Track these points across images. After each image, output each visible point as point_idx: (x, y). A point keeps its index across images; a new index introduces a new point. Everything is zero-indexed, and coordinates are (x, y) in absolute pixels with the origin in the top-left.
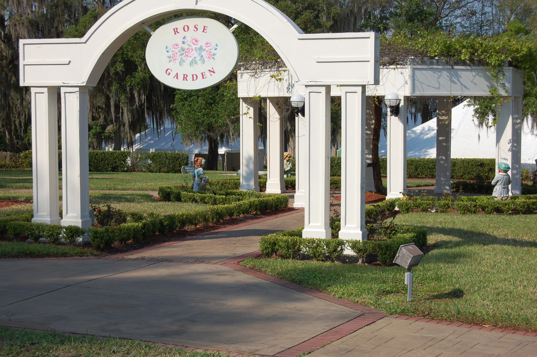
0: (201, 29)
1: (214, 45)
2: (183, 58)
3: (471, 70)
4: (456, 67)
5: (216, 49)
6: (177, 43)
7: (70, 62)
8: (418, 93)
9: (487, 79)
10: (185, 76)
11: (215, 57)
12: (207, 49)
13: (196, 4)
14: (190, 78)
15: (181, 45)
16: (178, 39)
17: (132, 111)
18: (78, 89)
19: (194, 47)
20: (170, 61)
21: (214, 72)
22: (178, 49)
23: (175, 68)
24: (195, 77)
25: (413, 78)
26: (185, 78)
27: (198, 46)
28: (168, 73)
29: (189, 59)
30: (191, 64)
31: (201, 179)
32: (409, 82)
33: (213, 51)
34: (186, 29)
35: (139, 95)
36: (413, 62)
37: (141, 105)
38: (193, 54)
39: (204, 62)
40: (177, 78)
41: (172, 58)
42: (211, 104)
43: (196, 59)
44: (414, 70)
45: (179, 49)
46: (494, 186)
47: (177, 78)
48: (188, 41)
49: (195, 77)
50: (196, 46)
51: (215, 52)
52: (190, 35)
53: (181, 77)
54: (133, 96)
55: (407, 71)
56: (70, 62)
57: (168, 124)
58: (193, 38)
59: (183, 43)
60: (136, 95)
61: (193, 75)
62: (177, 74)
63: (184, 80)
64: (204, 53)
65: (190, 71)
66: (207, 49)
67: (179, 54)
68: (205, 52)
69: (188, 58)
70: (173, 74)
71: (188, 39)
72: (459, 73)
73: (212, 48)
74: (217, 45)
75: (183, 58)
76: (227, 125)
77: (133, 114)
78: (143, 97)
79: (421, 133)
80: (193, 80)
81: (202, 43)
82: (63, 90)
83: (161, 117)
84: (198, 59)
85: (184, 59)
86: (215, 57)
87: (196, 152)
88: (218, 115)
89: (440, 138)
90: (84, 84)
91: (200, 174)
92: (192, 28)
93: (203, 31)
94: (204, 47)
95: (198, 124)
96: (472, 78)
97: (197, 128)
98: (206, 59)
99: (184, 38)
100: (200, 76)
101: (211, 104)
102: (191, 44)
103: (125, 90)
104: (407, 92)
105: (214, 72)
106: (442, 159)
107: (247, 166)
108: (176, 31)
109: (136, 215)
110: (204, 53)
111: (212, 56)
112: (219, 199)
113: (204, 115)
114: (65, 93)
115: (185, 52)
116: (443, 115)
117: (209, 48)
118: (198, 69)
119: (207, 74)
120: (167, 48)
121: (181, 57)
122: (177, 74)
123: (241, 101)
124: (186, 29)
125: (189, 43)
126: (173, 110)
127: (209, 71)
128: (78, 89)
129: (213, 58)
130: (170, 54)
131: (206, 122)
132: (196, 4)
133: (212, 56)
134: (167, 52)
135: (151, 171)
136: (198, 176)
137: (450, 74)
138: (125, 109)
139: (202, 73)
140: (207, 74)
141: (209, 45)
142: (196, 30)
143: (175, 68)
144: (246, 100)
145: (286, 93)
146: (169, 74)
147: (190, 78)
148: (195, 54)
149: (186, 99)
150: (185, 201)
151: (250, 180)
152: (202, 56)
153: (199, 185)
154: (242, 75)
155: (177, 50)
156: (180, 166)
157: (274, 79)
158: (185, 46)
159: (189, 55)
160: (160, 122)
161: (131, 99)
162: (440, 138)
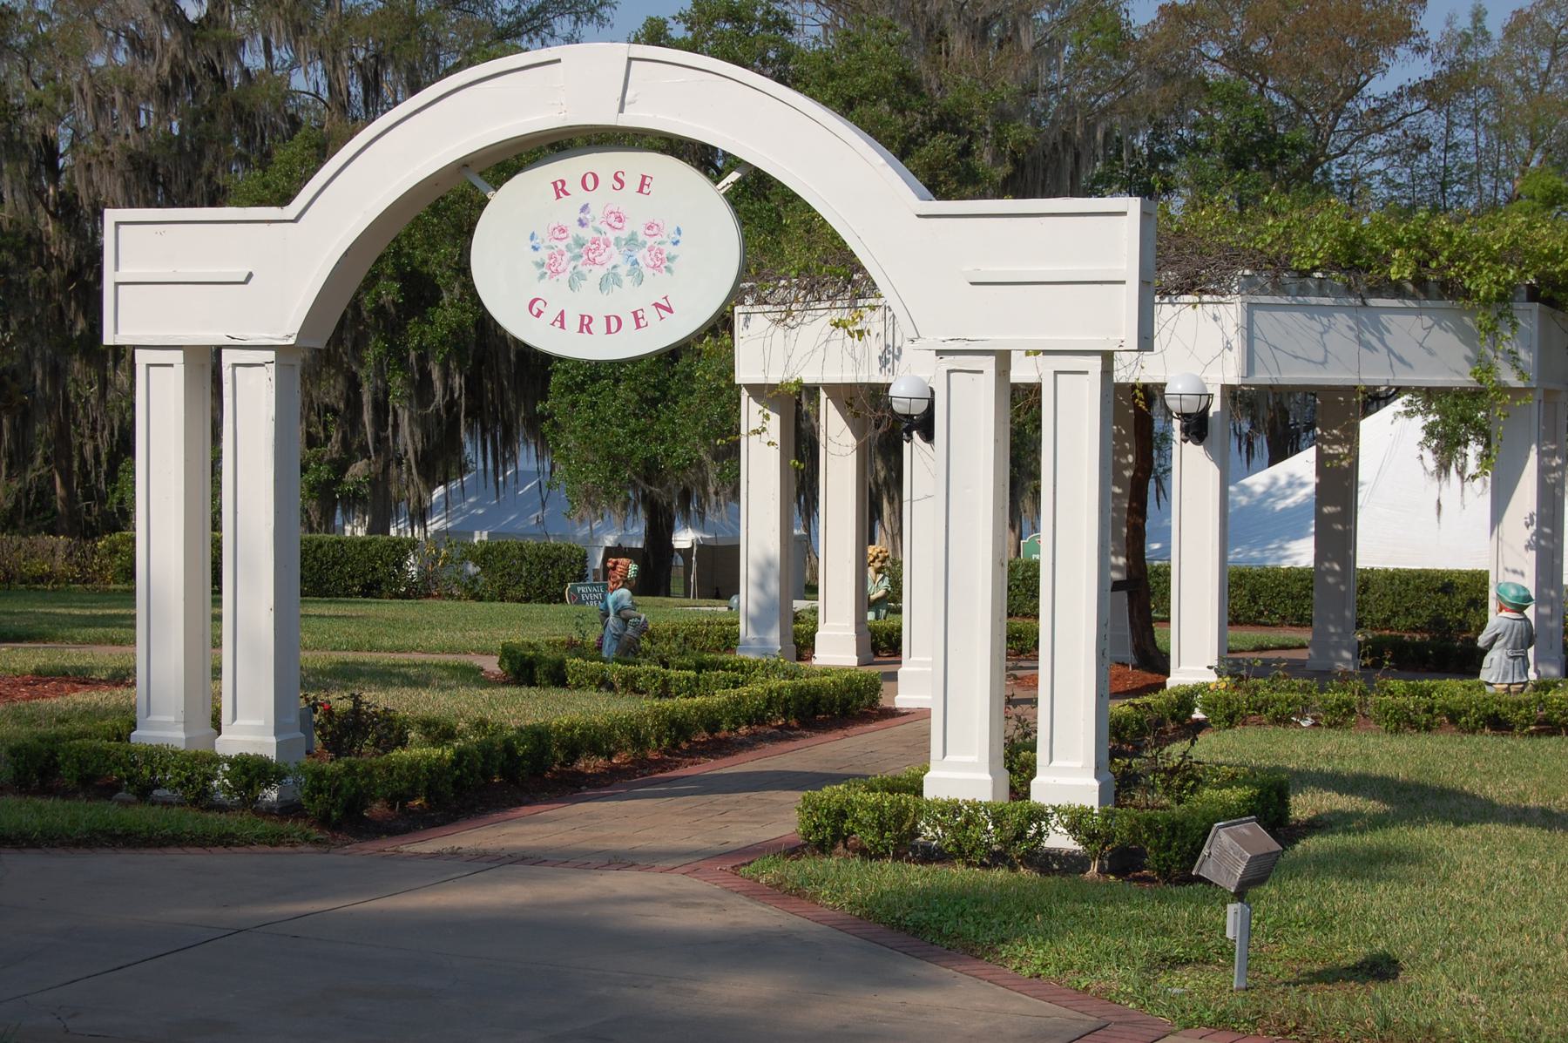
0: (632, 183)
1: (670, 229)
2: (580, 268)
3: (1419, 312)
4: (1373, 302)
5: (676, 243)
6: (564, 223)
7: (250, 275)
8: (1262, 377)
9: (1466, 337)
10: (586, 320)
12: (650, 242)
13: (621, 110)
14: (598, 326)
15: (574, 230)
17: (421, 422)
18: (271, 355)
19: (611, 235)
20: (543, 276)
21: (670, 310)
22: (565, 242)
23: (556, 295)
24: (613, 324)
25: (1249, 332)
26: (585, 325)
27: (625, 234)
28: (535, 311)
29: (599, 272)
30: (603, 284)
31: (626, 620)
32: (1237, 343)
33: (668, 249)
34: (590, 182)
35: (446, 375)
36: (1249, 286)
37: (451, 405)
38: (610, 257)
40: (562, 327)
41: (547, 269)
42: (654, 402)
43: (619, 270)
44: (1250, 308)
45: (570, 241)
46: (1484, 652)
47: (562, 327)
48: (594, 219)
49: (613, 324)
50: (618, 233)
51: (674, 250)
52: (602, 199)
53: (573, 322)
54: (426, 376)
55: (1231, 311)
56: (250, 275)
57: (526, 458)
58: (609, 209)
59: (582, 223)
60: (436, 374)
61: (608, 318)
62: (562, 314)
63: (581, 331)
66: (650, 242)
67: (568, 255)
68: (645, 251)
69: (595, 268)
70: (550, 314)
71: (596, 212)
72: (1384, 318)
73: (665, 238)
75: (580, 268)
76: (700, 464)
77: (426, 436)
78: (458, 381)
79: (1267, 494)
80: (609, 332)
82: (228, 358)
83: (508, 439)
84: (623, 270)
87: (610, 541)
88: (674, 435)
89: (1326, 510)
90: (291, 341)
91: (623, 608)
92: (606, 180)
93: (641, 191)
94: (641, 237)
95: (616, 462)
96: (1419, 333)
97: (615, 471)
98: (647, 272)
99: (584, 208)
100: (628, 321)
101: (654, 402)
103: (403, 361)
104: (1231, 372)
105: (670, 310)
106: (1332, 572)
107: (762, 586)
108: (560, 189)
109: (437, 725)
110: (641, 255)
111: (664, 263)
112: (678, 680)
113: (633, 433)
114: (235, 365)
115: (586, 251)
116: (1336, 441)
118: (624, 300)
119: (651, 315)
120: (532, 238)
121: (573, 264)
122: (562, 314)
123: (745, 394)
124: (590, 182)
125: (596, 224)
126: (543, 418)
127: (657, 305)
128: (271, 355)
129: (668, 269)
130: (543, 254)
131: (641, 454)
132: (621, 110)
133: (664, 263)
135: (479, 598)
136: (618, 613)
137: (1359, 322)
138: (404, 418)
139: (635, 313)
140: (651, 315)
141: (655, 230)
142: (618, 185)
143: (556, 295)
144: (757, 391)
145: (876, 373)
146: (540, 312)
147: (598, 326)
148: (614, 256)
149: (581, 387)
150: (578, 686)
151: (769, 627)
152: (636, 262)
153: (618, 638)
154: (747, 319)
155: (561, 245)
156: (563, 584)
157: (841, 332)
158: (587, 234)
159: (598, 260)
160: (503, 453)
161: (422, 388)
162: (1326, 510)
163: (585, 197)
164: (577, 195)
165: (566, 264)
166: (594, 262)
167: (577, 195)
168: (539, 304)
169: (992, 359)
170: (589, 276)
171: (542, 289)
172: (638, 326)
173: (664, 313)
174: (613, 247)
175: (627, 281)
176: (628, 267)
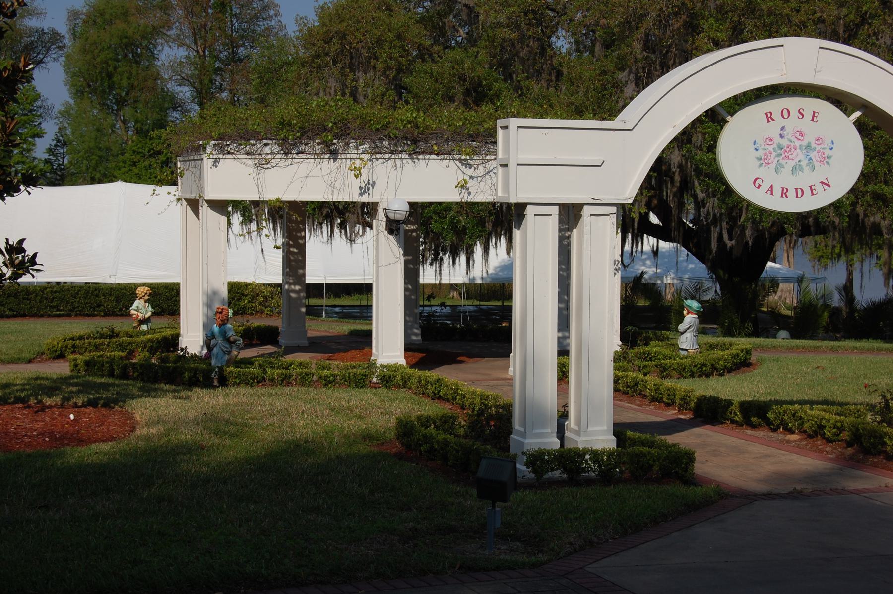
0: (808, 115)
1: (828, 142)
6: (772, 136)
11: (830, 161)
12: (818, 148)
15: (778, 140)
16: (773, 130)
19: (798, 144)
20: (761, 165)
21: (829, 185)
23: (768, 176)
24: (799, 193)
26: (784, 193)
27: (805, 143)
28: (757, 185)
29: (791, 163)
33: (828, 152)
38: (797, 156)
39: (813, 169)
40: (772, 194)
41: (763, 161)
43: (802, 163)
45: (775, 146)
47: (772, 194)
49: (799, 193)
50: (801, 143)
52: (792, 123)
53: (777, 191)
59: (781, 136)
61: (796, 189)
62: (772, 186)
64: (813, 155)
65: (792, 183)
66: (818, 148)
67: (774, 154)
68: (815, 152)
69: (789, 162)
70: (765, 186)
71: (789, 131)
74: (833, 143)
75: (781, 161)
80: (797, 197)
81: (810, 138)
84: (804, 163)
85: (783, 162)
86: (830, 161)
92: (794, 113)
93: (813, 120)
94: (813, 145)
98: (817, 164)
99: (783, 128)
100: (807, 191)
102: (794, 139)
105: (829, 185)
108: (769, 117)
110: (813, 155)
111: (826, 160)
115: (784, 152)
117: (822, 146)
118: (805, 179)
119: (819, 188)
121: (777, 159)
122: (772, 186)
124: (786, 114)
125: (789, 137)
127: (822, 182)
128: (614, 210)
130: (760, 153)
133: (826, 160)
134: (756, 150)
139: (811, 187)
140: (819, 188)
141: (820, 142)
142: (800, 116)
143: (768, 176)
147: (791, 193)
148: (799, 155)
152: (811, 159)
155: (771, 148)
158: (784, 142)
163: (783, 122)
166: (788, 158)
167: (779, 121)
168: (759, 181)
170: (785, 166)
171: (761, 172)
172: (813, 194)
173: (826, 187)
174: (798, 150)
176: (807, 161)
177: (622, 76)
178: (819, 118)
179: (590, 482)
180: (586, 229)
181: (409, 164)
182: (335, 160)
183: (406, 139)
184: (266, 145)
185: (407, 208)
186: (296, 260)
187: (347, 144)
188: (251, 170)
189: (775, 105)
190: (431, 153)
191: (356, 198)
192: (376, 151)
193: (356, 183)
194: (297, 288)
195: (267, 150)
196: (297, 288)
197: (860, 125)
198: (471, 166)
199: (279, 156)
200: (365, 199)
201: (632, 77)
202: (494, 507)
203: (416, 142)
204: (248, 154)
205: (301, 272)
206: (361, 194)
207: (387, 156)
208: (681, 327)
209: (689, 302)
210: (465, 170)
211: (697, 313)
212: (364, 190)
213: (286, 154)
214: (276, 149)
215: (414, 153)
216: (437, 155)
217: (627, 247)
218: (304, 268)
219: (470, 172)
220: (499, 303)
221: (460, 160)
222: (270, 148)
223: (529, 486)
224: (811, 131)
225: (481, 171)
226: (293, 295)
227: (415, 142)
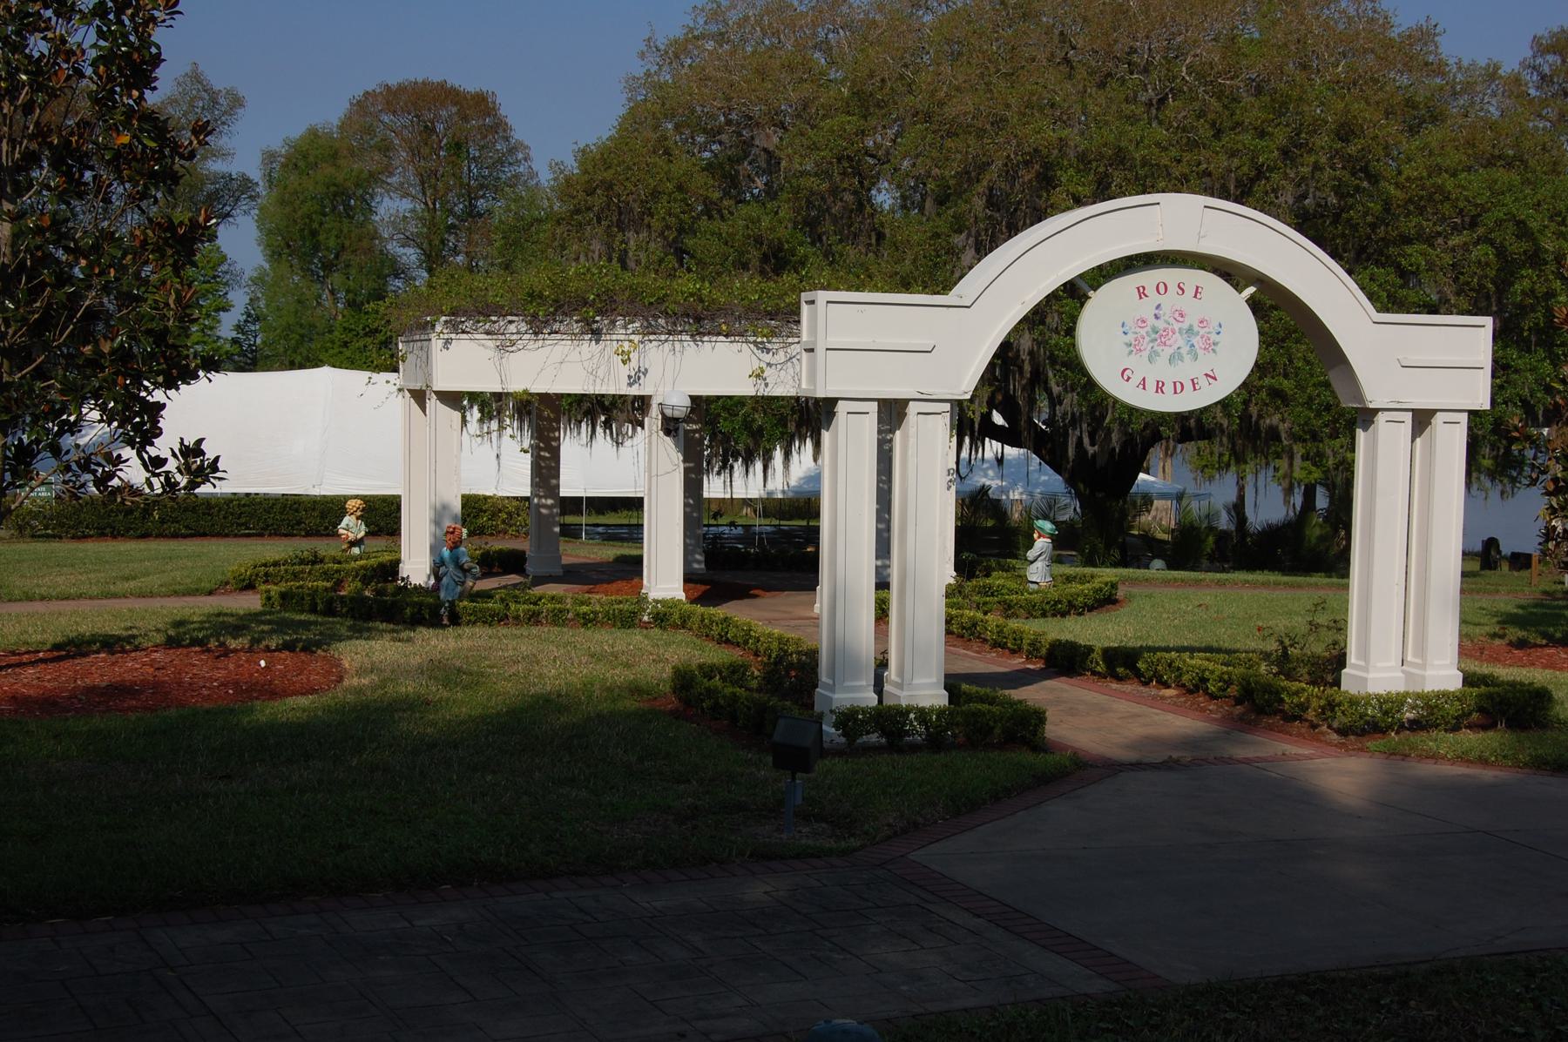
0: (1190, 292)
11: (1217, 348)
12: (1202, 332)
14: (1168, 388)
15: (1151, 321)
16: (1146, 308)
19: (1176, 326)
23: (1140, 367)
24: (1178, 388)
26: (1160, 387)
27: (1185, 326)
29: (1169, 351)
33: (1214, 337)
41: (1133, 348)
49: (1178, 388)
52: (1170, 301)
59: (1157, 317)
64: (1196, 340)
65: (1169, 375)
66: (1202, 332)
70: (1136, 379)
71: (1166, 311)
81: (1191, 320)
85: (1159, 349)
92: (1173, 288)
94: (1196, 328)
98: (1201, 353)
99: (1158, 307)
102: (1172, 321)
108: (1142, 292)
110: (1196, 340)
111: (1211, 347)
118: (1187, 370)
119: (1203, 382)
128: (947, 406)
130: (1130, 338)
133: (1211, 347)
140: (1203, 382)
147: (1168, 388)
148: (1179, 341)
155: (1143, 332)
158: (1160, 324)
164: (1154, 298)
165: (1146, 345)
167: (1154, 298)
168: (1128, 373)
169: (1466, 415)
175: (1187, 358)
177: (958, 240)
178: (1203, 294)
179: (914, 748)
180: (912, 431)
181: (690, 347)
182: (597, 341)
183: (688, 316)
184: (511, 322)
185: (688, 402)
186: (549, 468)
187: (613, 322)
188: (491, 353)
189: (1149, 278)
190: (719, 334)
191: (624, 390)
192: (649, 331)
193: (624, 371)
194: (550, 502)
195: (512, 328)
196: (550, 502)
197: (1254, 304)
198: (768, 351)
199: (527, 336)
200: (634, 391)
201: (972, 240)
202: (794, 779)
203: (699, 320)
204: (488, 333)
205: (554, 482)
206: (630, 385)
207: (663, 337)
208: (1031, 554)
209: (1040, 523)
210: (761, 356)
211: (1051, 536)
212: (633, 380)
213: (536, 334)
214: (523, 327)
215: (697, 334)
216: (726, 336)
217: (965, 454)
218: (558, 477)
219: (767, 358)
220: (804, 523)
221: (755, 343)
222: (517, 326)
223: (838, 752)
224: (1194, 311)
225: (781, 357)
226: (544, 511)
227: (698, 319)
